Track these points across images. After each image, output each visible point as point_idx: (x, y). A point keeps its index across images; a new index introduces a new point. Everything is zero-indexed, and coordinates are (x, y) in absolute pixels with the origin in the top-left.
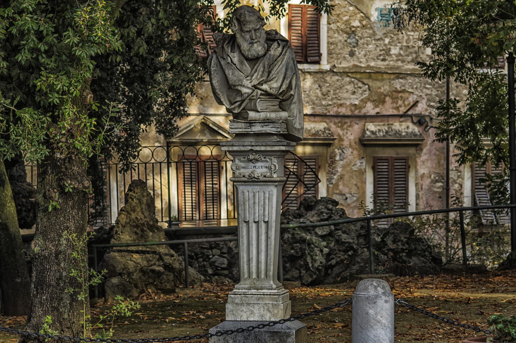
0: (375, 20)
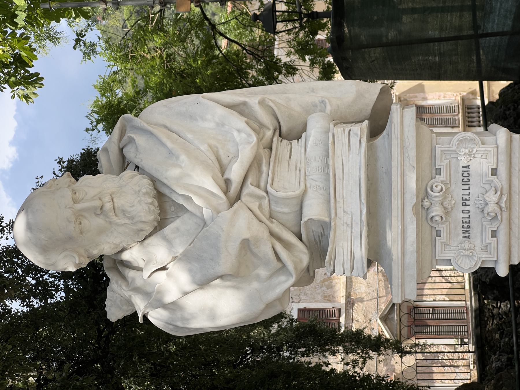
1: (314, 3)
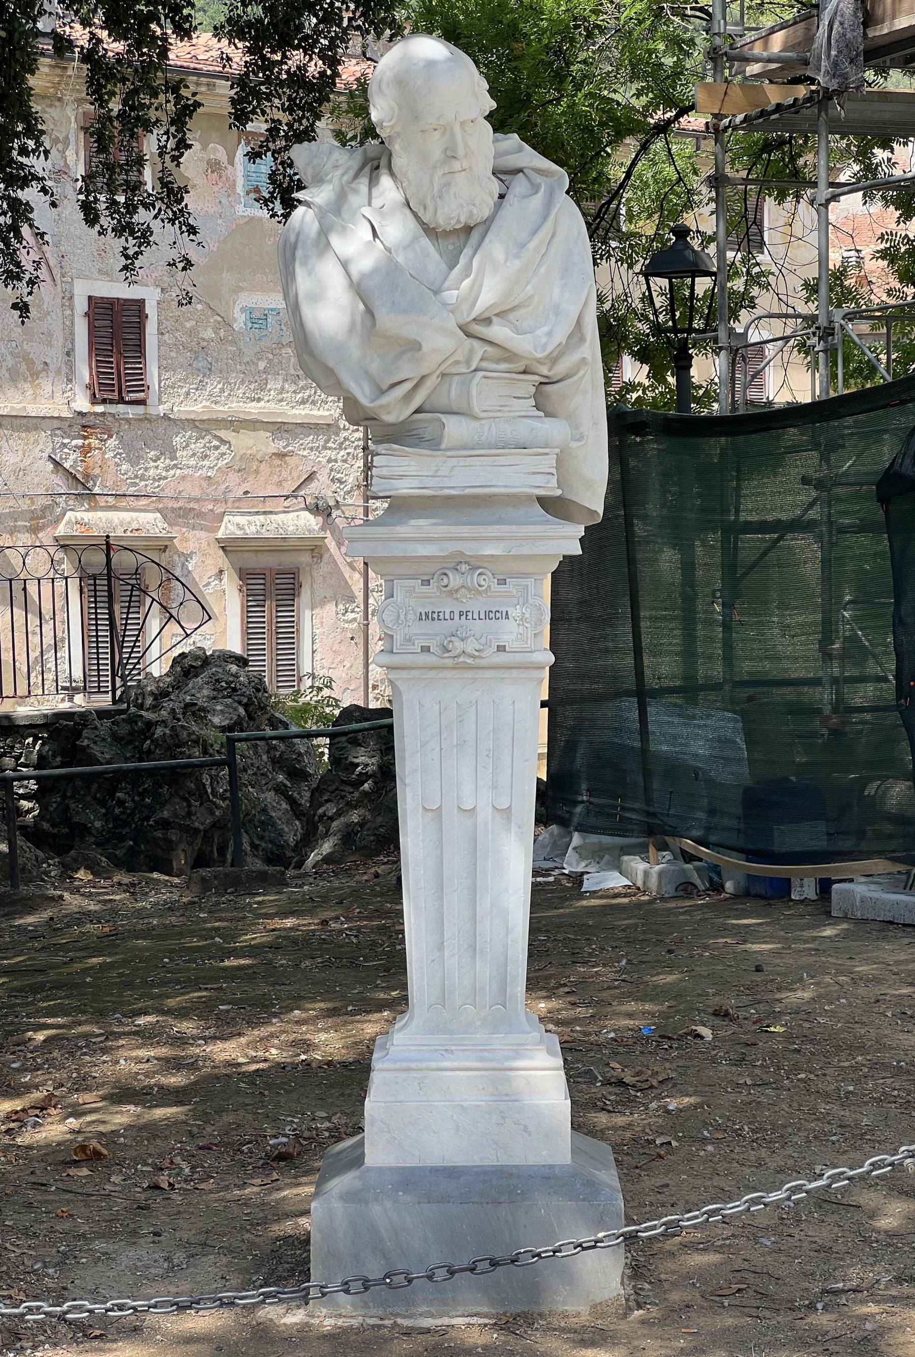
0: (241, 328)
1: (710, 355)
